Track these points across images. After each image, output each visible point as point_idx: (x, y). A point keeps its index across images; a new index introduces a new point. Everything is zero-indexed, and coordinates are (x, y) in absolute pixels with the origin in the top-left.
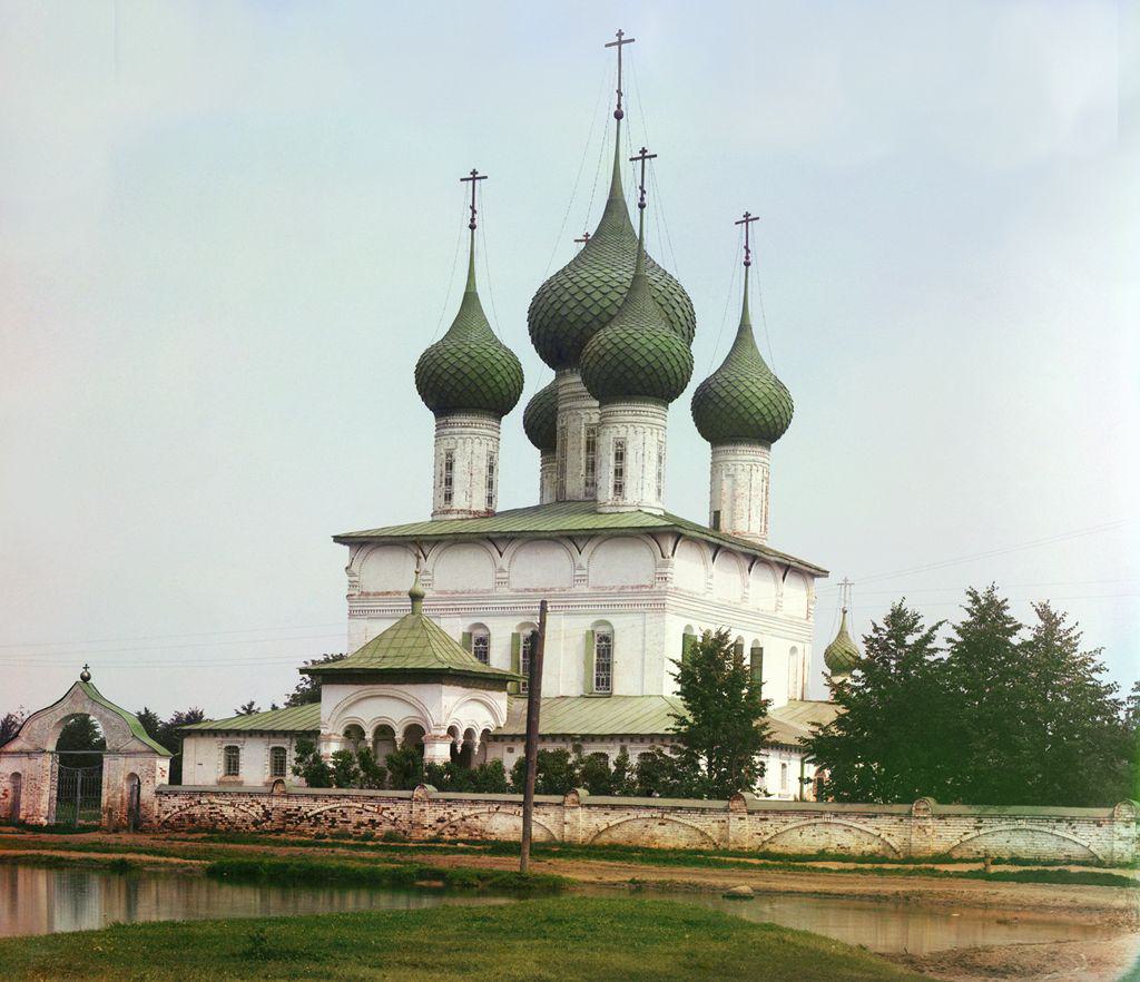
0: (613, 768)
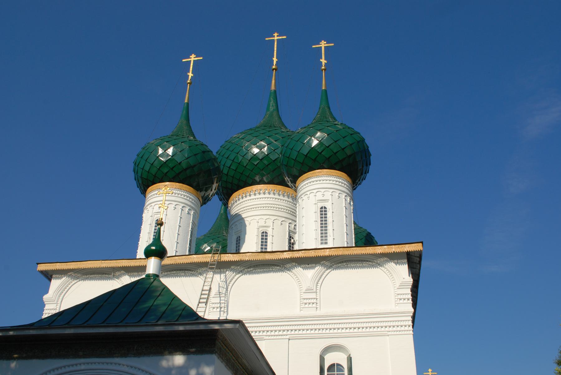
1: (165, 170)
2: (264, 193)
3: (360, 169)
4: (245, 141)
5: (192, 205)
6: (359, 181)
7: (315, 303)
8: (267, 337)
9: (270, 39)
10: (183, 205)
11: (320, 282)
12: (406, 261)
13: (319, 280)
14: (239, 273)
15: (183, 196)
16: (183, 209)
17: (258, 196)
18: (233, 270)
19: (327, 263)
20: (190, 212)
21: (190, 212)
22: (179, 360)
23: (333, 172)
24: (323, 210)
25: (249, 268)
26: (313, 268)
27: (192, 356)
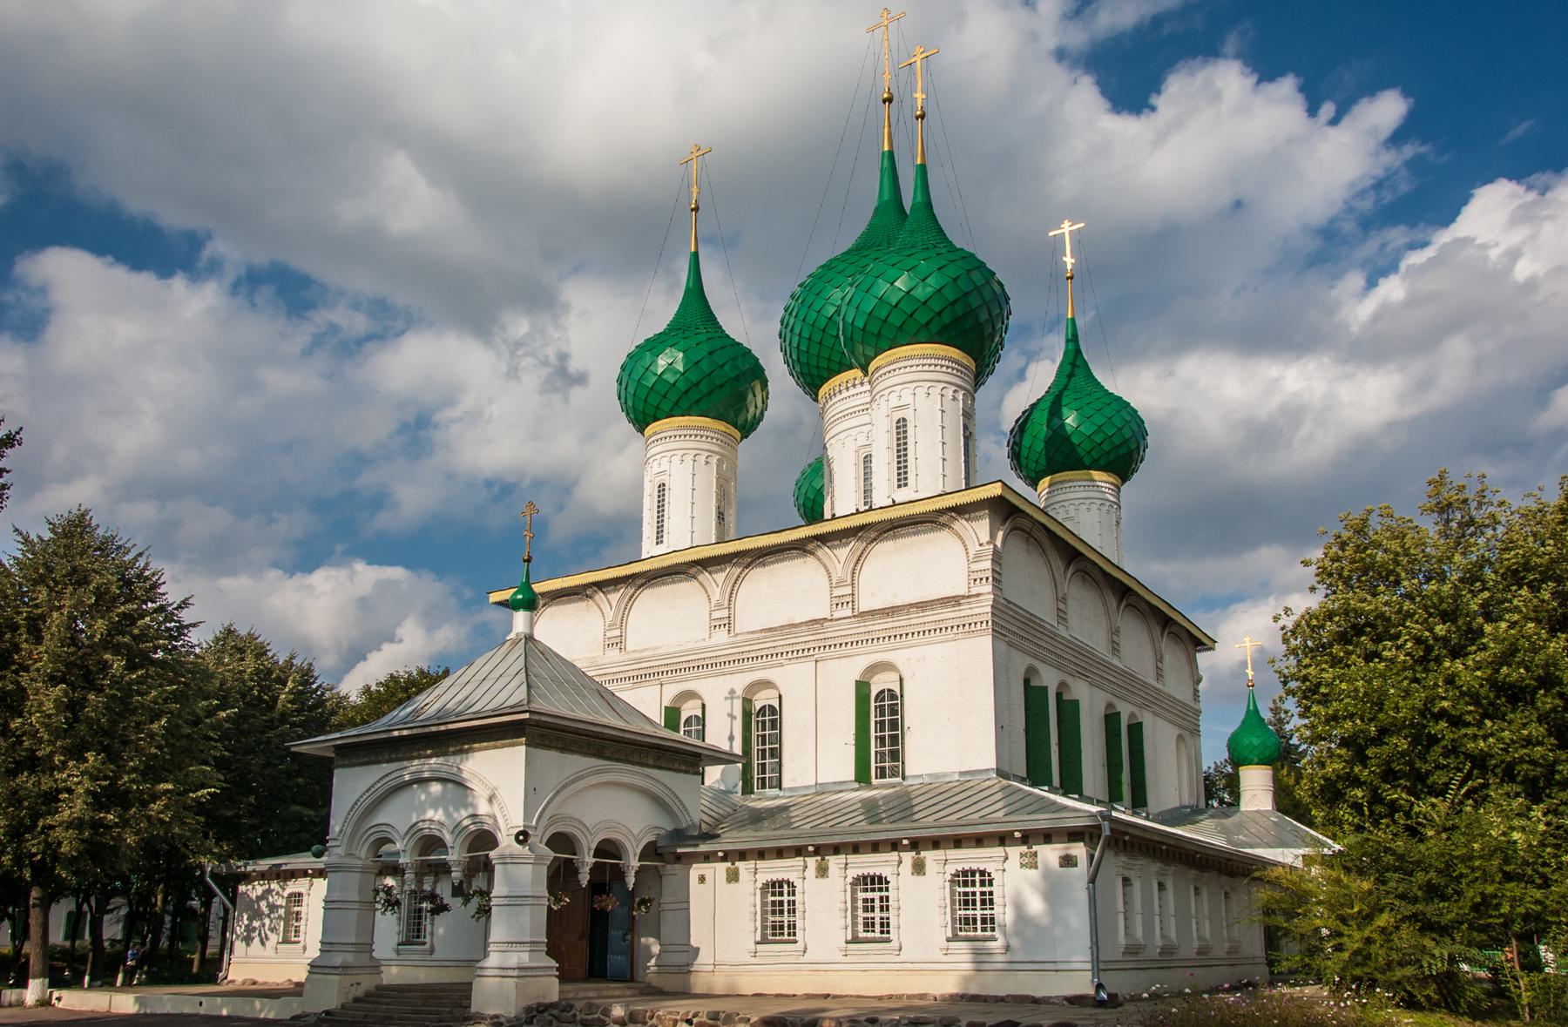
1: (654, 400)
2: (862, 384)
3: (998, 315)
4: (829, 287)
5: (959, 382)
6: (1003, 323)
17: (852, 391)
20: (956, 395)
26: (723, 570)
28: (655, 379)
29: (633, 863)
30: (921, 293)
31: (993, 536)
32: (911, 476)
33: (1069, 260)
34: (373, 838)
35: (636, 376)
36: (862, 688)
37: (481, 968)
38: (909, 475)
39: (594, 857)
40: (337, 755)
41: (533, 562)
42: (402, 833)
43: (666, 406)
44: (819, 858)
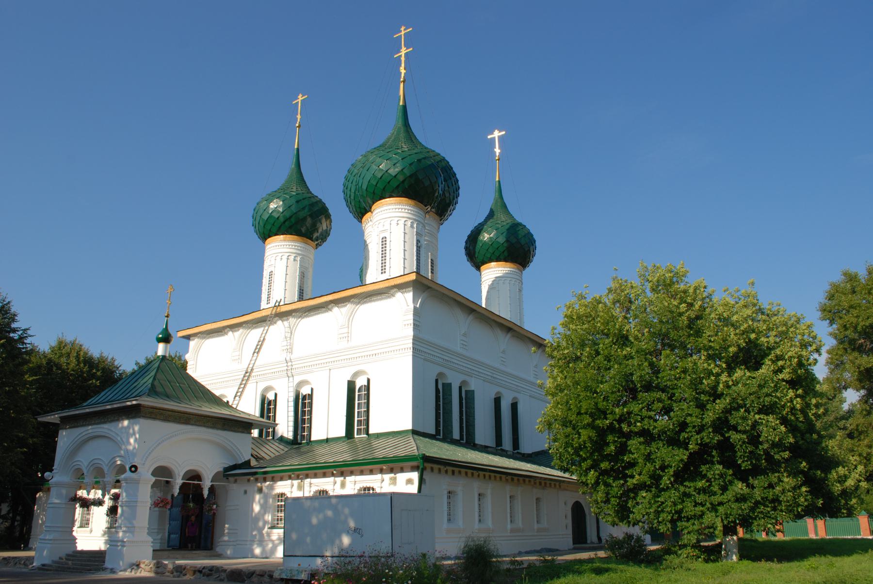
0: (206, 493)
1: (268, 227)
7: (348, 337)
8: (317, 370)
9: (397, 35)
10: (295, 255)
11: (351, 318)
12: (411, 289)
13: (351, 316)
14: (358, 304)
15: (288, 246)
16: (406, 223)
18: (294, 317)
19: (356, 300)
21: (296, 259)
22: (126, 423)
23: (391, 201)
24: (384, 240)
25: (305, 313)
27: (131, 420)
28: (268, 215)
29: (206, 484)
30: (393, 171)
31: (415, 301)
32: (387, 267)
33: (497, 151)
34: (73, 469)
35: (259, 214)
36: (351, 386)
37: (221, 541)
38: (386, 267)
39: (182, 480)
40: (61, 422)
41: (170, 317)
42: (107, 463)
43: (274, 230)
44: (300, 481)
